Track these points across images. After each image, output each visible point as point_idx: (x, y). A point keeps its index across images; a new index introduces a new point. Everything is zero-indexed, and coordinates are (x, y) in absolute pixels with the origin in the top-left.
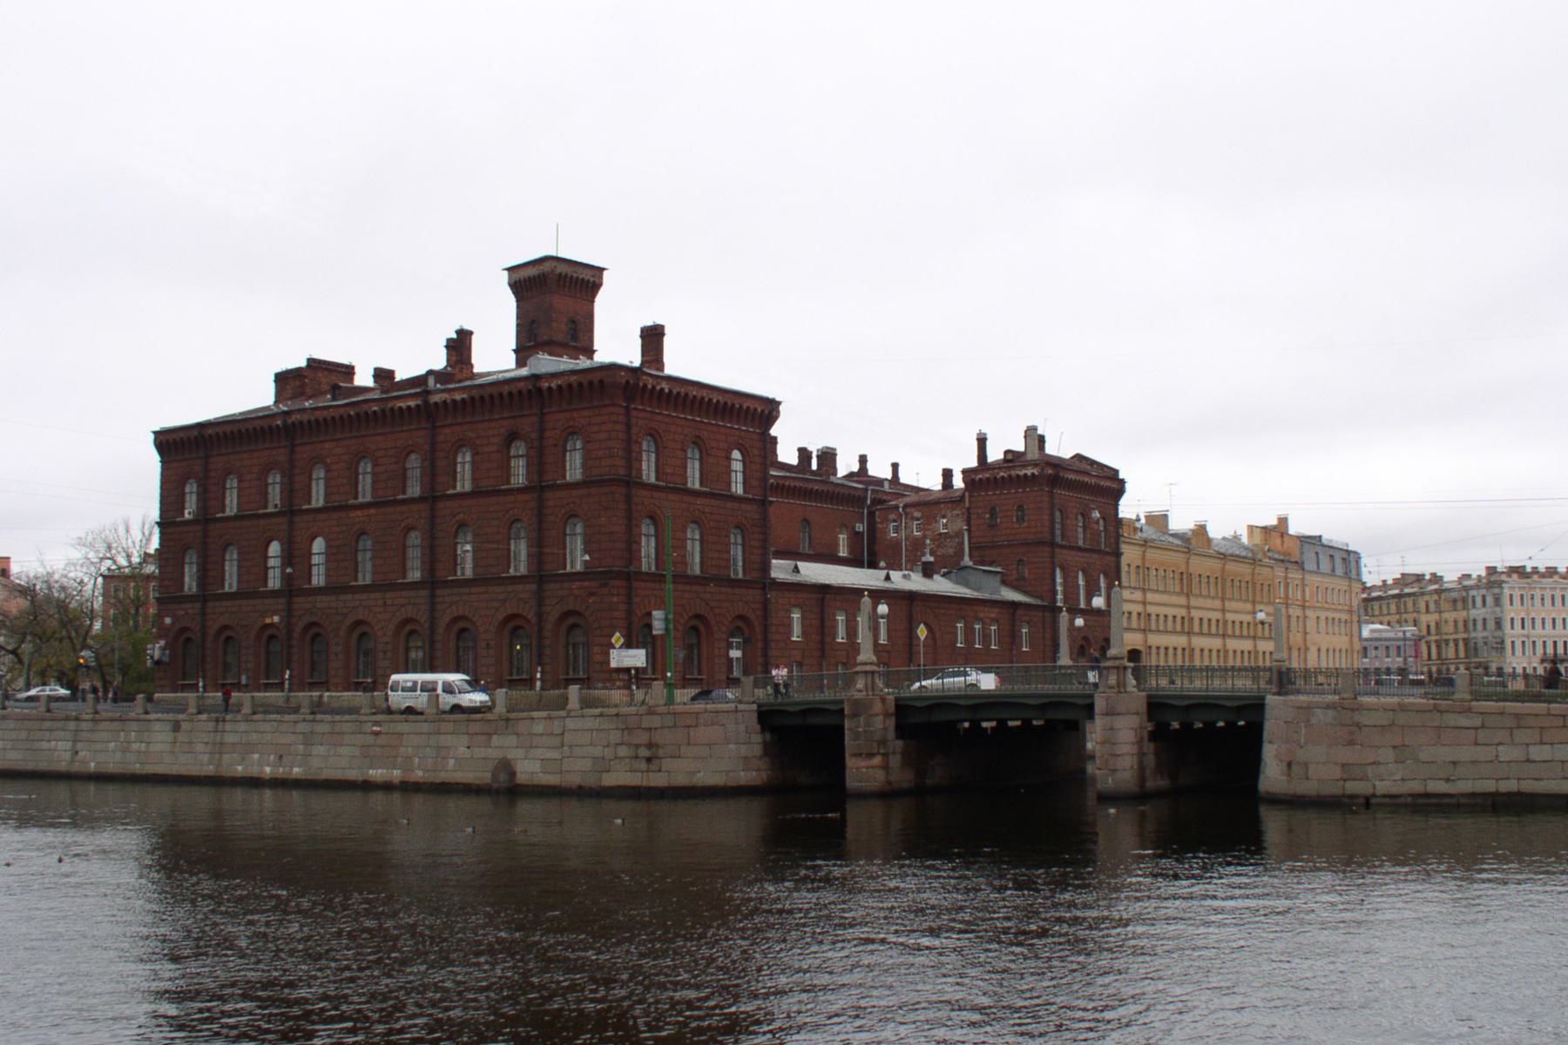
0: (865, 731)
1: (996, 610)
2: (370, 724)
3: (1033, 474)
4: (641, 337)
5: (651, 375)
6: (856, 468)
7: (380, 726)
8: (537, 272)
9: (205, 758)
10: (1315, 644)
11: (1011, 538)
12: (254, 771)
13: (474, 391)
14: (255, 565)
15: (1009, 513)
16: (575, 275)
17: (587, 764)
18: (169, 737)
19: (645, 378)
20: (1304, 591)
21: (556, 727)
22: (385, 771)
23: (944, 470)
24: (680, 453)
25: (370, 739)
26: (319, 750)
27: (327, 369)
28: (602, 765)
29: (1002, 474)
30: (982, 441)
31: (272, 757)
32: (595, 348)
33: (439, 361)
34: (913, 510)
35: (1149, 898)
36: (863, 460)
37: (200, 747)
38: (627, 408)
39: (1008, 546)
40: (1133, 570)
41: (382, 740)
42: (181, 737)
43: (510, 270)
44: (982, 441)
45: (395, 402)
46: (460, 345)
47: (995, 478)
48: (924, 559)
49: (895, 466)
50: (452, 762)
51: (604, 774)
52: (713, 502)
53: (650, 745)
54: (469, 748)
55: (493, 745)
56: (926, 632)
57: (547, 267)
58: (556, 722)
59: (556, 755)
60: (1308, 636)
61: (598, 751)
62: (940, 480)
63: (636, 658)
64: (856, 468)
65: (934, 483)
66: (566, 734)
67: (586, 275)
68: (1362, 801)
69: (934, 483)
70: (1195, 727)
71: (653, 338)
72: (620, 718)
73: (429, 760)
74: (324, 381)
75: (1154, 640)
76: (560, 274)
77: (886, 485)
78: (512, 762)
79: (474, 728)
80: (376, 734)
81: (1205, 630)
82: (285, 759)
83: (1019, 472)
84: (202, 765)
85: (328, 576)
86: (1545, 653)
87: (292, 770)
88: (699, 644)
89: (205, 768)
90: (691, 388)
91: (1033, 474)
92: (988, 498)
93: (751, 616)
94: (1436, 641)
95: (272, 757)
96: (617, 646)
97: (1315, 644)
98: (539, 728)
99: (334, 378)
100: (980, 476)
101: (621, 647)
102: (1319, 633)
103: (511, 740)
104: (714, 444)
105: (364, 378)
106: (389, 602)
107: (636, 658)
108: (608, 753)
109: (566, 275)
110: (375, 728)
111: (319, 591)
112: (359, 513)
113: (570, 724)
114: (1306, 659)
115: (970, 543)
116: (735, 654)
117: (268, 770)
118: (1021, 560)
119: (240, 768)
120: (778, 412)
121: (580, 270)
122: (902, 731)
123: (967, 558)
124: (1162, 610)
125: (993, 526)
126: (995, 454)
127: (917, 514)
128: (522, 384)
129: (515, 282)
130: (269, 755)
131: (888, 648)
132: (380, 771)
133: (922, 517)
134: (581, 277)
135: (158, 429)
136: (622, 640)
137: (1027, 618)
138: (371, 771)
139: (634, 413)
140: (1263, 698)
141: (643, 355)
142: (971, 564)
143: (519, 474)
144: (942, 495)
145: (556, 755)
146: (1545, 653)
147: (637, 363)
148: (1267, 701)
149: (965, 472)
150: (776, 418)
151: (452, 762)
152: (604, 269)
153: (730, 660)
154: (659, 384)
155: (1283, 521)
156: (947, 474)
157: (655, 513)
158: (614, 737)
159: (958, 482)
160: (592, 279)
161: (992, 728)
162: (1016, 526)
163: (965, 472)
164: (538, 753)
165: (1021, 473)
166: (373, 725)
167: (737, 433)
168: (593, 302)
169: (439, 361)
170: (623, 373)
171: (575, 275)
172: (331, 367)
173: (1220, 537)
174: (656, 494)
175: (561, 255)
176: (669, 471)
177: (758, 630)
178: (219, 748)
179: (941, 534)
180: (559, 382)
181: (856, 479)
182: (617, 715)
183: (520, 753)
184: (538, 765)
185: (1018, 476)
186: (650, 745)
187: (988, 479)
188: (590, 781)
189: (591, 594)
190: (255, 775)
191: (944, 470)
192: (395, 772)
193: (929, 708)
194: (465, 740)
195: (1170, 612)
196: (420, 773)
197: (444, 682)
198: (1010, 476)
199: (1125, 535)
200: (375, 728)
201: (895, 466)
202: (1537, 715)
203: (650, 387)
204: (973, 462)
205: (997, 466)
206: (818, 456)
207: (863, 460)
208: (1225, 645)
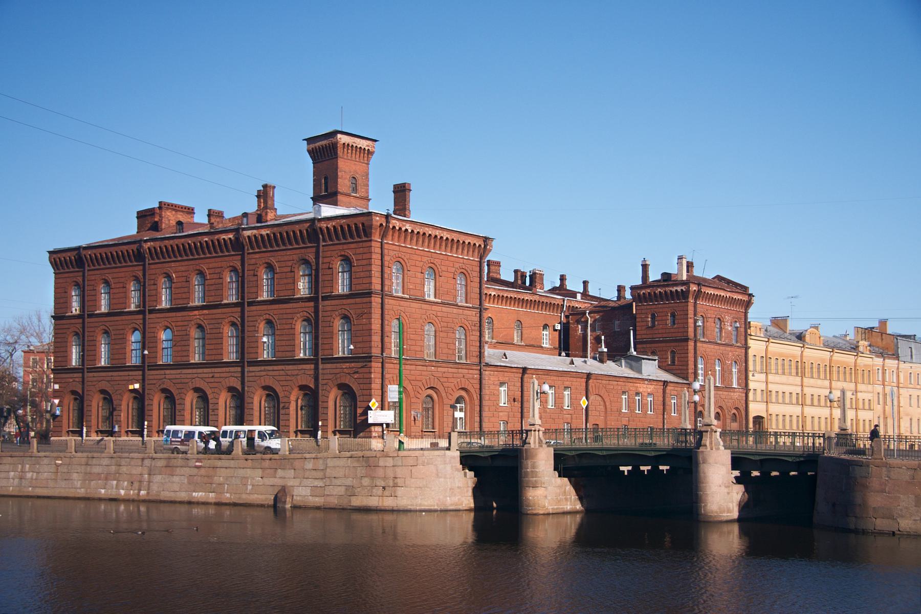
1: (652, 387)
4: (394, 192)
5: (398, 220)
6: (558, 284)
7: (201, 462)
9: (79, 484)
10: (907, 415)
11: (665, 335)
13: (301, 225)
14: (284, 340)
17: (341, 491)
19: (394, 221)
20: (898, 376)
21: (320, 464)
22: (204, 494)
24: (419, 275)
25: (195, 471)
26: (158, 478)
29: (659, 290)
30: (645, 267)
31: (126, 483)
33: (252, 206)
36: (563, 278)
37: (75, 476)
38: (381, 243)
40: (758, 359)
41: (203, 471)
43: (310, 141)
44: (645, 267)
45: (220, 235)
46: (265, 195)
49: (585, 283)
50: (250, 487)
51: (352, 497)
52: (444, 309)
54: (261, 478)
55: (277, 476)
56: (581, 402)
58: (321, 461)
59: (319, 483)
60: (901, 409)
61: (349, 482)
63: (388, 417)
64: (558, 284)
65: (612, 295)
69: (612, 295)
70: (752, 475)
71: (401, 192)
72: (365, 458)
73: (145, 483)
74: (172, 218)
75: (774, 409)
77: (579, 296)
79: (267, 464)
81: (787, 401)
83: (671, 289)
85: (174, 356)
88: (433, 408)
90: (427, 229)
91: (682, 290)
92: (648, 307)
93: (469, 388)
95: (126, 483)
96: (373, 408)
97: (907, 415)
98: (309, 465)
99: (179, 216)
100: (644, 291)
101: (376, 409)
102: (911, 406)
104: (444, 268)
105: (201, 218)
107: (388, 417)
108: (355, 482)
109: (348, 145)
111: (104, 369)
112: (196, 312)
113: (330, 463)
114: (899, 426)
115: (634, 338)
116: (459, 415)
117: (122, 492)
119: (103, 491)
123: (632, 350)
124: (781, 388)
126: (654, 276)
130: (124, 481)
131: (571, 412)
132: (200, 493)
135: (52, 249)
136: (377, 404)
137: (675, 393)
138: (194, 494)
139: (386, 246)
141: (395, 206)
142: (635, 353)
143: (303, 287)
145: (319, 483)
149: (632, 288)
151: (250, 487)
153: (454, 420)
154: (405, 226)
156: (620, 289)
159: (628, 295)
161: (628, 471)
163: (632, 288)
164: (309, 482)
165: (674, 289)
166: (196, 462)
167: (461, 261)
169: (252, 206)
170: (378, 218)
173: (831, 336)
174: (402, 303)
176: (411, 287)
177: (475, 398)
178: (89, 477)
179: (615, 332)
180: (334, 224)
181: (557, 292)
183: (295, 482)
184: (309, 491)
188: (344, 503)
190: (472, 498)
193: (579, 456)
194: (259, 472)
195: (788, 389)
196: (228, 495)
197: (199, 432)
199: (752, 334)
201: (585, 283)
202: (226, 468)
203: (397, 228)
205: (656, 284)
206: (530, 276)
207: (563, 278)
208: (857, 416)
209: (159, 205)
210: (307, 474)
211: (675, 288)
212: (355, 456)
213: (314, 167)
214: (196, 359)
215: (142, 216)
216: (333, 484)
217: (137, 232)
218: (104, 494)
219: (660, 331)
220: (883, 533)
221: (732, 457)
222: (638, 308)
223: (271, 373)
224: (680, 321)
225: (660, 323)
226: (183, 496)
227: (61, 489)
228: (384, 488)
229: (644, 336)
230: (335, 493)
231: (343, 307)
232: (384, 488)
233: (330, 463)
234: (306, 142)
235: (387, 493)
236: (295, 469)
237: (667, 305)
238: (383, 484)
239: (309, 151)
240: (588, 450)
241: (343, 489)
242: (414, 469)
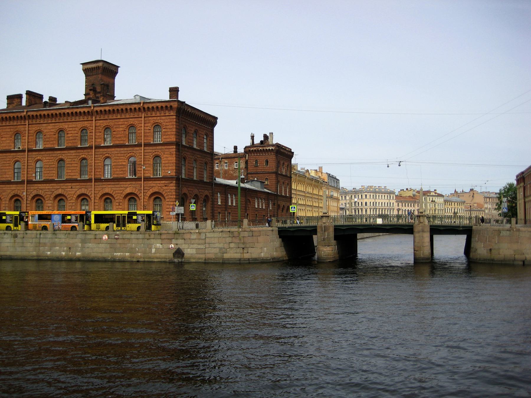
0: (327, 238)
2: (114, 235)
3: (272, 149)
4: (169, 91)
8: (96, 66)
12: (57, 254)
13: (114, 107)
15: (262, 162)
16: (110, 68)
18: (12, 240)
23: (234, 146)
27: (34, 95)
28: (223, 251)
29: (261, 149)
30: (253, 137)
32: (115, 96)
34: (225, 160)
35: (361, 294)
39: (262, 173)
41: (120, 241)
42: (18, 240)
44: (253, 137)
47: (258, 150)
48: (241, 177)
53: (244, 243)
54: (161, 244)
57: (100, 64)
59: (202, 247)
61: (221, 245)
62: (233, 150)
65: (231, 151)
66: (206, 239)
67: (113, 68)
68: (521, 263)
76: (105, 67)
78: (182, 250)
80: (117, 239)
82: (72, 250)
83: (266, 148)
84: (29, 252)
86: (379, 214)
87: (76, 254)
89: (31, 253)
91: (272, 149)
92: (254, 157)
94: (354, 209)
103: (180, 241)
106: (73, 187)
108: (226, 246)
109: (107, 68)
110: (116, 237)
118: (267, 178)
119: (49, 253)
120: (217, 122)
121: (111, 66)
122: (336, 238)
125: (256, 166)
126: (257, 141)
127: (226, 161)
128: (136, 105)
129: (86, 69)
130: (64, 247)
132: (119, 254)
133: (228, 162)
134: (111, 69)
138: (115, 254)
140: (472, 226)
144: (233, 155)
145: (202, 247)
146: (379, 214)
147: (168, 98)
148: (473, 228)
150: (217, 124)
152: (119, 67)
155: (321, 168)
157: (186, 156)
158: (229, 240)
160: (115, 70)
162: (265, 166)
164: (195, 246)
165: (268, 148)
168: (114, 78)
171: (110, 68)
172: (36, 95)
175: (102, 59)
182: (229, 232)
183: (186, 246)
184: (195, 251)
185: (266, 149)
186: (244, 243)
187: (255, 150)
189: (166, 186)
191: (234, 146)
192: (127, 254)
198: (263, 149)
200: (116, 237)
204: (249, 143)
205: (257, 146)
209: (90, 88)
210: (193, 242)
211: (269, 148)
212: (225, 231)
213: (86, 78)
214: (108, 176)
215: (10, 98)
216: (211, 247)
217: (7, 107)
218: (50, 254)
219: (261, 168)
220: (18, 259)
221: (430, 228)
222: (249, 157)
223: (109, 186)
224: (271, 164)
225: (260, 164)
226: (108, 255)
227: (19, 252)
228: (243, 248)
229: (252, 171)
230: (212, 252)
231: (133, 151)
232: (243, 248)
233: (208, 235)
234: (82, 65)
235: (245, 251)
236: (184, 239)
237: (264, 156)
238: (243, 246)
239: (84, 70)
240: (303, 228)
241: (218, 250)
242: (259, 238)
